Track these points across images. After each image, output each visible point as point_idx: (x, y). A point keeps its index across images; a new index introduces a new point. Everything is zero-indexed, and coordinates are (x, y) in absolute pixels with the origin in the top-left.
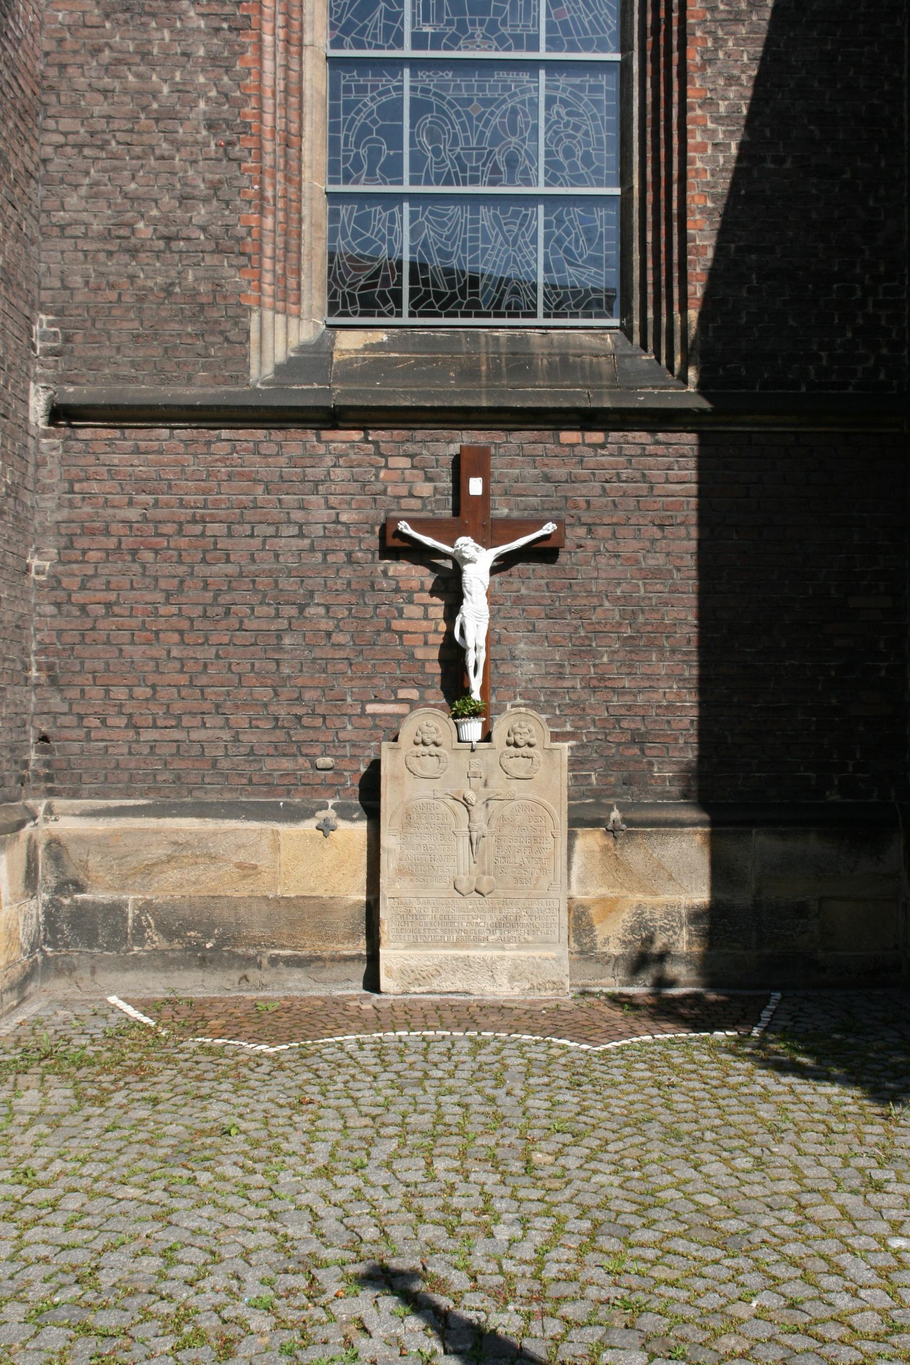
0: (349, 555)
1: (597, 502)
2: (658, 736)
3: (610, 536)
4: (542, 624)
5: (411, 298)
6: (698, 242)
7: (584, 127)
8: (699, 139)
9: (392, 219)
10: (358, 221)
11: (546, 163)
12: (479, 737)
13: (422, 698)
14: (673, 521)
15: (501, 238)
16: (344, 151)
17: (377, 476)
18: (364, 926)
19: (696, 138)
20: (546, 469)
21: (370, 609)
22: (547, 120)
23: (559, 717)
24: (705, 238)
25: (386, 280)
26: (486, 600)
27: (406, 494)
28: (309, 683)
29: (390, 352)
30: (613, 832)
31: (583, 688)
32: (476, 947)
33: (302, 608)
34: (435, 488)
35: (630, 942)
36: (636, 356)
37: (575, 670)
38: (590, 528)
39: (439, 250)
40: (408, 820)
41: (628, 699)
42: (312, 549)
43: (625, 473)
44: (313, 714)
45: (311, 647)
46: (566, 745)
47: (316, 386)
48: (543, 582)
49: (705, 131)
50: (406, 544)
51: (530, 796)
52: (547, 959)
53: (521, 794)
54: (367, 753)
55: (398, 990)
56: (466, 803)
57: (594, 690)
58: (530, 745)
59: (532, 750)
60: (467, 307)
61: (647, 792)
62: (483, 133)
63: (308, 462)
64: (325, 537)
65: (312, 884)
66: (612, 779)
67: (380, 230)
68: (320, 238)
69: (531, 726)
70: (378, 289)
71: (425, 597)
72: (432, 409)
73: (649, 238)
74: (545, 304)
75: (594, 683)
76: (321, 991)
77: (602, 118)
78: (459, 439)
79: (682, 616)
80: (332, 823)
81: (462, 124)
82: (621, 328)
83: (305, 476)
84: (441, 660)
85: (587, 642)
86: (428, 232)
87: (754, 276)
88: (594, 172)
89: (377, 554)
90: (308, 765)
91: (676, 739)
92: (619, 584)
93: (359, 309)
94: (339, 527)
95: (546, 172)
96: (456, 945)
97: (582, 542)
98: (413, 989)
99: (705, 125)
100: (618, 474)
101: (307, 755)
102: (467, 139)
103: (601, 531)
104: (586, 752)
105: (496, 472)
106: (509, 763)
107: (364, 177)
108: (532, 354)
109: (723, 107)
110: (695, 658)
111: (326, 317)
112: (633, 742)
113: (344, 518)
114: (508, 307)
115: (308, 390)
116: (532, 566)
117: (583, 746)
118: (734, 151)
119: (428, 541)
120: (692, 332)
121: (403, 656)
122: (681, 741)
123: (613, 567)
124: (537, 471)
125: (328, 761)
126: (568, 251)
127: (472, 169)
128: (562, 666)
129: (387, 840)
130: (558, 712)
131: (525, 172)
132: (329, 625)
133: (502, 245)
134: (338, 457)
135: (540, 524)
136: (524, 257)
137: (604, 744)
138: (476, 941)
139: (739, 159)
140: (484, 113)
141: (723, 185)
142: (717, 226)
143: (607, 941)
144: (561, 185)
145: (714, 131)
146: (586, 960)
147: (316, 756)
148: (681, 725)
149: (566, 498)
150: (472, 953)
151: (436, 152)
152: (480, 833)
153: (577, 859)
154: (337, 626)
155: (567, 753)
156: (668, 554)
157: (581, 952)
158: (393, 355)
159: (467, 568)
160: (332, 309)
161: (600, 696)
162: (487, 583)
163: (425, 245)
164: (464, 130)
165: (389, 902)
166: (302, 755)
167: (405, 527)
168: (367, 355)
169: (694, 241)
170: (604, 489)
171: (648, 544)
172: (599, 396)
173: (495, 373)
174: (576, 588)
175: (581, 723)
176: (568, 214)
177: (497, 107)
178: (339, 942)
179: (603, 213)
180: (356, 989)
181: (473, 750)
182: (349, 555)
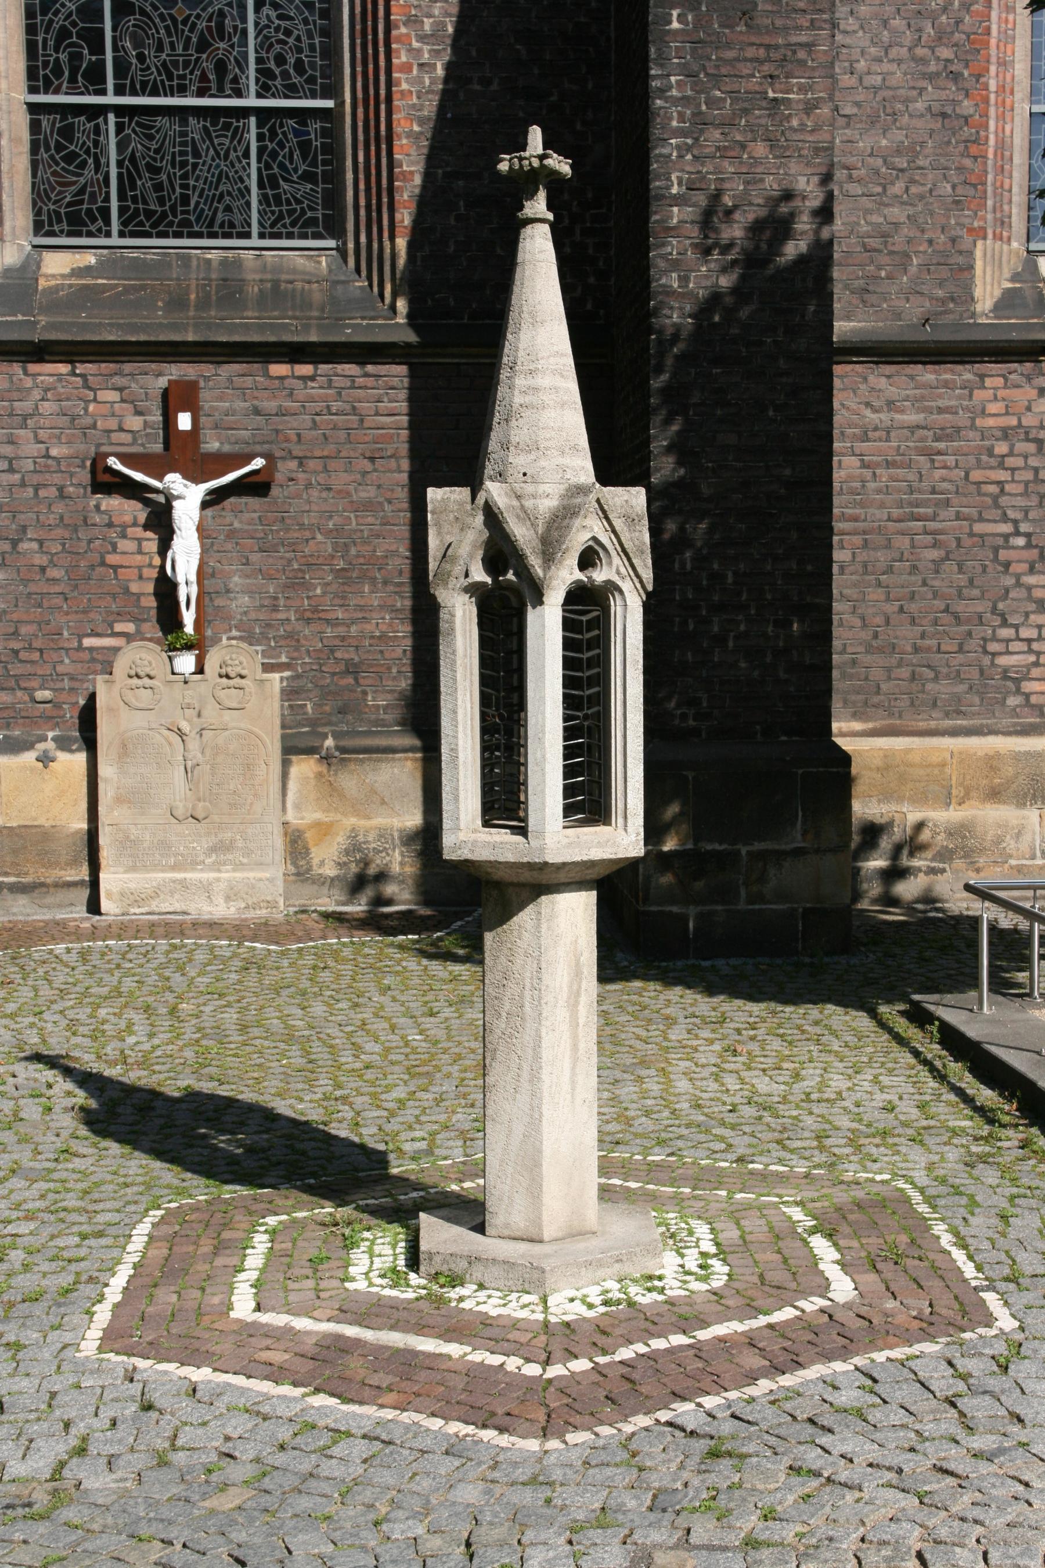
0: (61, 489)
1: (307, 435)
2: (372, 666)
3: (321, 468)
4: (255, 557)
5: (120, 217)
6: (405, 168)
7: (296, 32)
8: (404, 59)
9: (97, 131)
10: (61, 132)
11: (257, 71)
12: (193, 669)
13: (138, 631)
14: (384, 454)
15: (212, 152)
16: (43, 55)
17: (86, 410)
18: (86, 852)
19: (401, 58)
20: (256, 402)
21: (84, 544)
22: (257, 24)
23: (274, 648)
24: (412, 163)
25: (93, 197)
26: (196, 535)
27: (116, 427)
28: (25, 618)
29: (97, 278)
30: (327, 759)
31: (297, 620)
32: (193, 870)
33: (15, 543)
34: (145, 422)
35: (345, 863)
36: (348, 282)
37: (289, 602)
38: (301, 461)
39: (148, 165)
40: (124, 750)
41: (341, 630)
42: (23, 484)
43: (335, 406)
44: (30, 648)
45: (25, 582)
46: (276, 676)
47: (20, 317)
48: (256, 515)
49: (411, 50)
50: (117, 480)
51: (243, 725)
52: (261, 880)
53: (234, 724)
54: (85, 685)
55: (117, 911)
56: (181, 734)
57: (308, 621)
58: (242, 677)
59: (243, 681)
60: (178, 226)
61: (362, 720)
62: (189, 39)
63: (15, 395)
64: (35, 471)
65: (34, 814)
66: (327, 708)
67: (84, 143)
68: (21, 153)
69: (242, 658)
70: (85, 206)
71: (139, 532)
72: (138, 343)
73: (361, 158)
74: (260, 223)
75: (308, 614)
76: (47, 916)
77: (314, 22)
78: (167, 372)
79: (393, 548)
80: (51, 754)
81: (167, 28)
82: (337, 249)
83: (13, 410)
84: (156, 594)
85: (300, 575)
86: (136, 145)
87: (462, 203)
88: (307, 81)
89: (89, 489)
90: (27, 698)
91: (389, 668)
92: (331, 517)
93: (66, 228)
94: (50, 462)
95: (257, 80)
96: (174, 868)
97: (294, 475)
98: (132, 911)
99: (410, 44)
100: (328, 407)
101: (25, 689)
102: (173, 48)
103: (312, 464)
104: (302, 682)
105: (206, 406)
106: (222, 694)
107: (65, 85)
108: (243, 280)
109: (428, 24)
110: (407, 589)
111: (31, 237)
112: (347, 672)
113: (54, 452)
114: (222, 226)
115: (12, 322)
116: (244, 500)
117: (298, 677)
118: (440, 71)
119: (138, 476)
120: (402, 261)
121: (118, 590)
122: (394, 670)
123: (325, 500)
124: (247, 404)
125: (47, 694)
126: (282, 166)
127: (180, 77)
128: (276, 598)
129: (105, 770)
130: (273, 644)
131: (235, 80)
132: (44, 560)
133: (213, 160)
134: (46, 390)
135: (248, 459)
136: (236, 172)
137: (319, 675)
138: (193, 864)
139: (446, 80)
140: (190, 15)
141: (430, 107)
142: (425, 151)
143: (322, 863)
144: (274, 96)
145: (419, 51)
146: (302, 881)
147: (34, 690)
148: (394, 655)
149: (277, 431)
150: (188, 875)
151: (141, 58)
152: (195, 762)
153: (292, 786)
154: (51, 561)
155: (277, 687)
156: (379, 487)
157: (298, 874)
158: (100, 281)
159: (176, 504)
160: (38, 228)
161: (315, 627)
162: (196, 518)
163: (133, 159)
164: (169, 35)
165: (107, 829)
166: (21, 689)
167: (114, 463)
168: (74, 281)
169: (401, 166)
170: (314, 422)
171: (359, 476)
172: (307, 328)
173: (203, 304)
174: (288, 521)
175: (296, 654)
176: (281, 126)
177: (204, 10)
178: (62, 869)
179: (318, 125)
180: (80, 912)
181: (186, 682)
182: (61, 489)
